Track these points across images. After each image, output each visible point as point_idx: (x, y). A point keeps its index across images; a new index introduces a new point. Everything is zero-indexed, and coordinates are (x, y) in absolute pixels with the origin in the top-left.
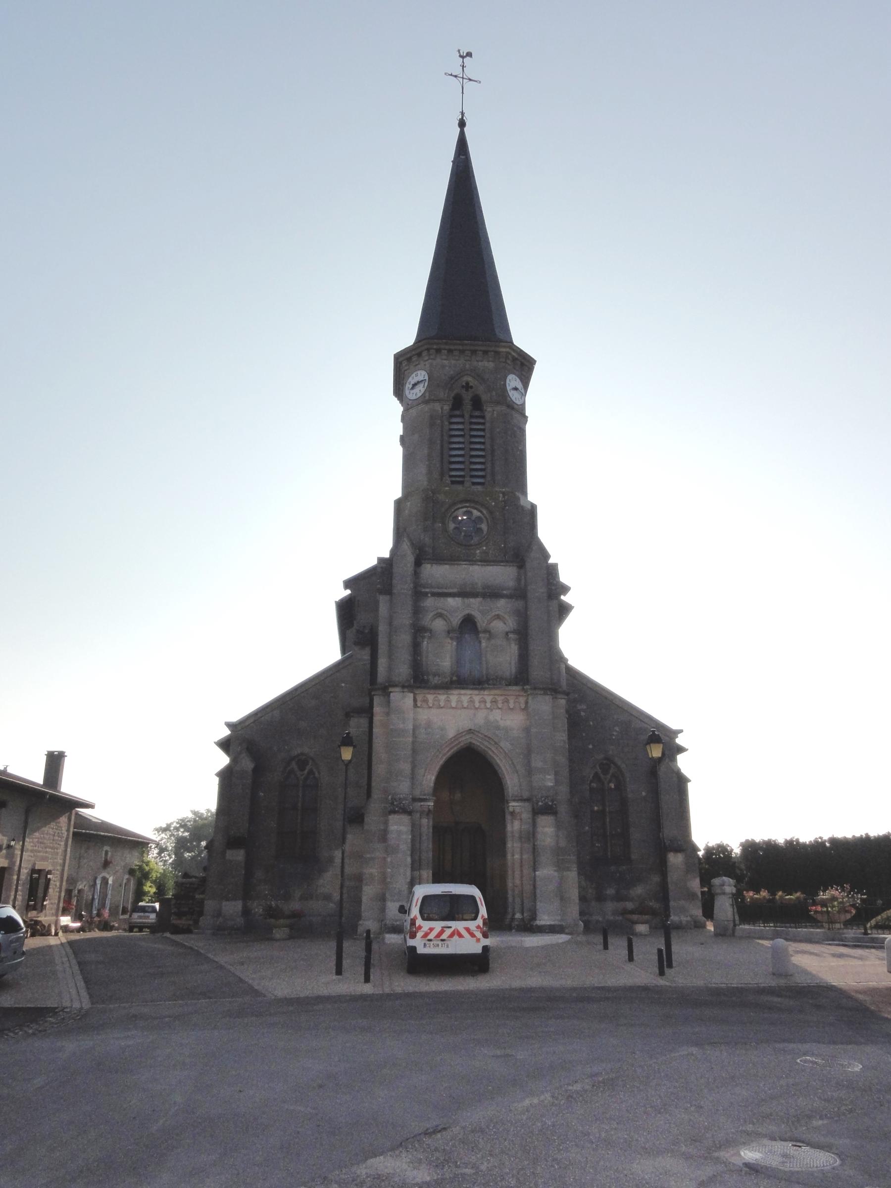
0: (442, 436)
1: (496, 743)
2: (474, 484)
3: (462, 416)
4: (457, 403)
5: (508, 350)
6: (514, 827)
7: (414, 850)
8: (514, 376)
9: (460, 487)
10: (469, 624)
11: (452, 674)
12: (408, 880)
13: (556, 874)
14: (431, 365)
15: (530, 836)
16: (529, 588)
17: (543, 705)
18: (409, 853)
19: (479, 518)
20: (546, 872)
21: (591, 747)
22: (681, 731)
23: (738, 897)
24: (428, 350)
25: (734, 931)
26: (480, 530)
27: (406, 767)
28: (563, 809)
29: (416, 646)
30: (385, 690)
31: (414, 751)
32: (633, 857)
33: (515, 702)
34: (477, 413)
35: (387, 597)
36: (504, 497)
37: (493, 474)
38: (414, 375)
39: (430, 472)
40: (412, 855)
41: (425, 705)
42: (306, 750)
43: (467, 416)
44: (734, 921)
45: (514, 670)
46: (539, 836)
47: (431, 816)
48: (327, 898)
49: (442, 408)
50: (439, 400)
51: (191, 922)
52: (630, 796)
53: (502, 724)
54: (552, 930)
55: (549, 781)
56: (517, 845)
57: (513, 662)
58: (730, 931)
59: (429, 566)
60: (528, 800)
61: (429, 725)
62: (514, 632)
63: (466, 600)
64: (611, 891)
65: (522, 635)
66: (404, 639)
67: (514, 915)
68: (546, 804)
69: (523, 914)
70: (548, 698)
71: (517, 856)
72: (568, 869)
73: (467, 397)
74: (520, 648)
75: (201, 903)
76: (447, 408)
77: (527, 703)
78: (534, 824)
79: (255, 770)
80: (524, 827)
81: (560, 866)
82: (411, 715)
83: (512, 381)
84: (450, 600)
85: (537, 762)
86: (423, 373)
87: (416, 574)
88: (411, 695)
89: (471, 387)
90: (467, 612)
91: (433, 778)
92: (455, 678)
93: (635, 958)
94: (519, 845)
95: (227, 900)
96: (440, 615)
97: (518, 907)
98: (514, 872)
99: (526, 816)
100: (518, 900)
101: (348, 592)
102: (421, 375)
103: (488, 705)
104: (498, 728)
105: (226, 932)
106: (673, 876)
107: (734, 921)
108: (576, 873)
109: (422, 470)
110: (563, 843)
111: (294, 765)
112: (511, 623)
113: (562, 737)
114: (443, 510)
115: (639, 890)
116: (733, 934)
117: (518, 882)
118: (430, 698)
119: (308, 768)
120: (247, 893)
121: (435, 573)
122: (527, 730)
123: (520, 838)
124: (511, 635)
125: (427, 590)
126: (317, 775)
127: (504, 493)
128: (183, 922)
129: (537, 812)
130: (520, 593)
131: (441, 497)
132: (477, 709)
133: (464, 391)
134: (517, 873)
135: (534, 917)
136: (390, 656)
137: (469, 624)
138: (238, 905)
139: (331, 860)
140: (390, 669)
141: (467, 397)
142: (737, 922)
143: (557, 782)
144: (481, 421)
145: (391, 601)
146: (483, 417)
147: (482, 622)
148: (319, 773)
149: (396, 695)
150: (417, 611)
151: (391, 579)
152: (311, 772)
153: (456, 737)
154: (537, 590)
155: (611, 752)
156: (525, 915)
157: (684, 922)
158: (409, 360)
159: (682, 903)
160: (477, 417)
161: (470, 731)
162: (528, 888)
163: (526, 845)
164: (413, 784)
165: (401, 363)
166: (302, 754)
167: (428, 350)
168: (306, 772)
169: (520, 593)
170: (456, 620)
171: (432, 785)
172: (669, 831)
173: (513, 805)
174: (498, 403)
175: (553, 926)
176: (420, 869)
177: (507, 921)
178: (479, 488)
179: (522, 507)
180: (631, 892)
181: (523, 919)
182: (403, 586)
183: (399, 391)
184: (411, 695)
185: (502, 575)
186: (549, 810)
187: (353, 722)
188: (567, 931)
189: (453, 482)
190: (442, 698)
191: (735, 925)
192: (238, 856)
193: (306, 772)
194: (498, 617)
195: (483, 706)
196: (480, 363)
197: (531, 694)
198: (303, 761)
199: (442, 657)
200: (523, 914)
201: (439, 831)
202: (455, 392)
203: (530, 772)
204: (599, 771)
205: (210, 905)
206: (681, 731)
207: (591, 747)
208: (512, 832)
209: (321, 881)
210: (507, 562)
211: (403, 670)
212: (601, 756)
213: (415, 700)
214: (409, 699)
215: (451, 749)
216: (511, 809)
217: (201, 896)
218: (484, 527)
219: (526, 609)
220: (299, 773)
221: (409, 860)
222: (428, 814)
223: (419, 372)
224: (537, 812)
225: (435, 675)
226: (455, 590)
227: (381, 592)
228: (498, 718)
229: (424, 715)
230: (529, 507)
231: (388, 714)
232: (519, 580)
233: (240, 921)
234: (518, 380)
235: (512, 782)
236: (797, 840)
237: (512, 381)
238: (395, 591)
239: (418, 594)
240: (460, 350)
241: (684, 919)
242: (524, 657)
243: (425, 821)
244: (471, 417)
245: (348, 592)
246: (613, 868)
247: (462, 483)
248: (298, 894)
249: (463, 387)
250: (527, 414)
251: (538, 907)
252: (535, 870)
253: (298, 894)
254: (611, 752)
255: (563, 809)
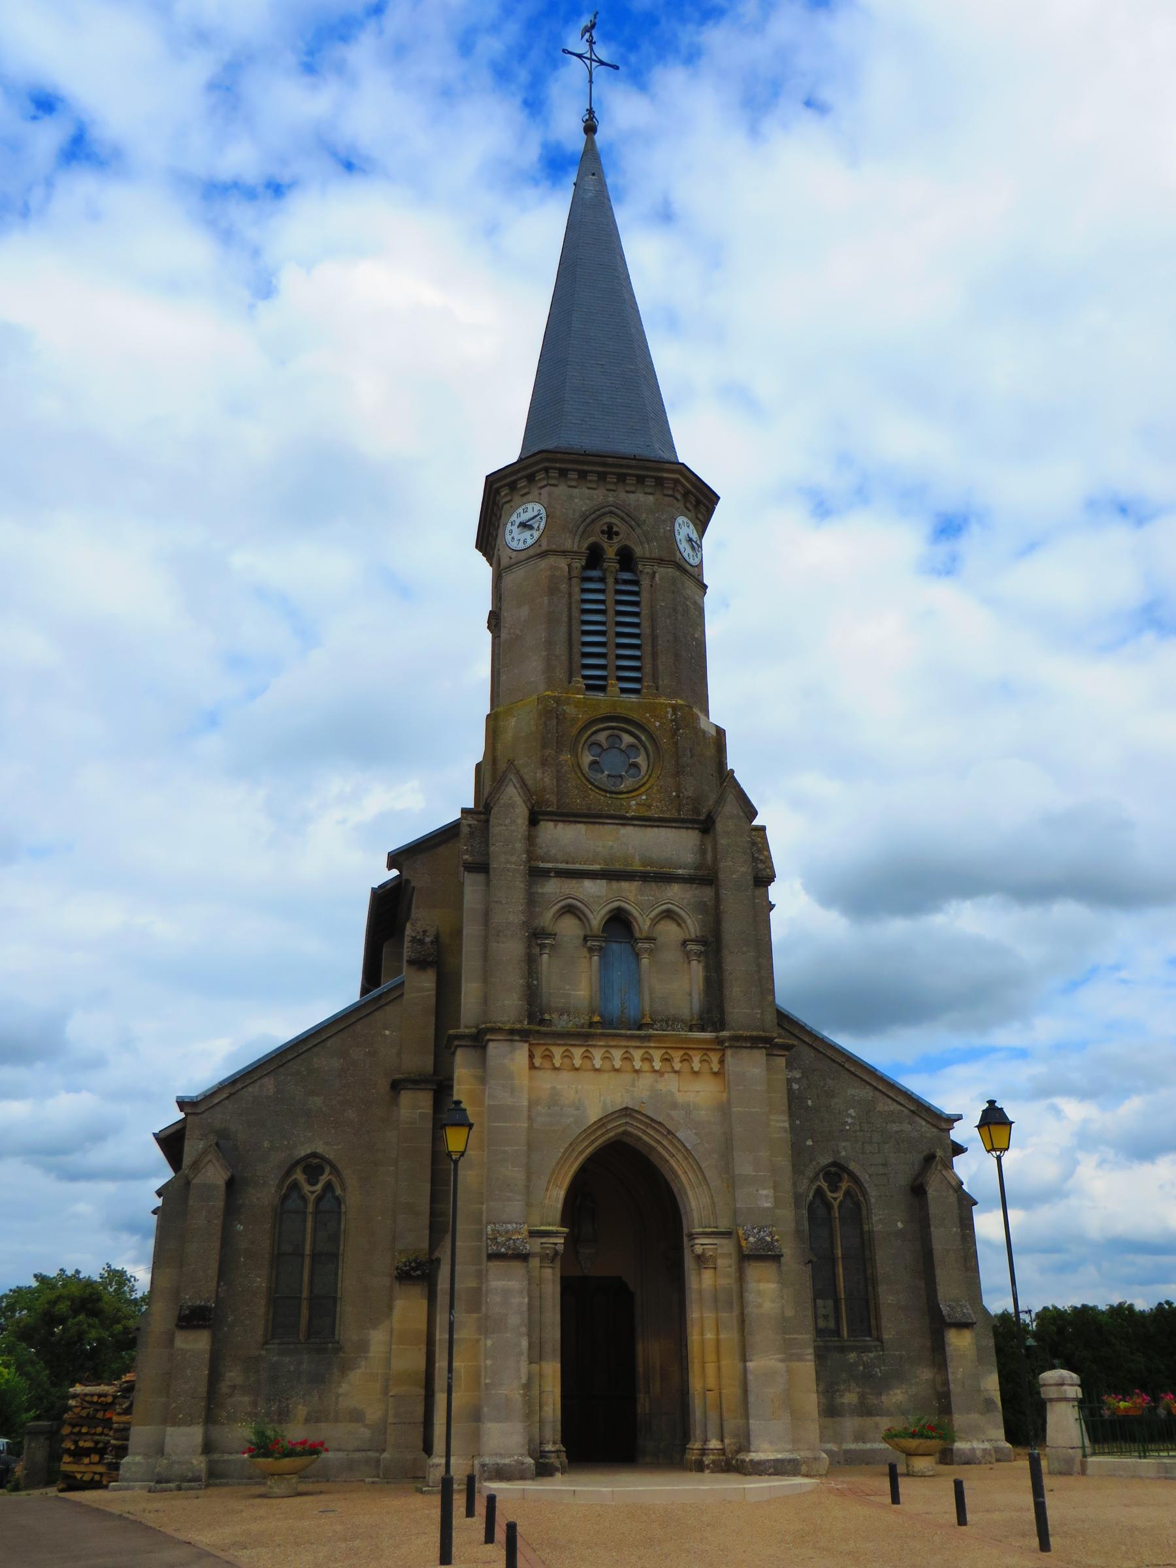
0: (570, 609)
1: (669, 1132)
2: (623, 691)
3: (602, 580)
4: (594, 557)
5: (677, 476)
6: (702, 1283)
7: (533, 1326)
8: (685, 520)
9: (600, 695)
10: (619, 922)
11: (593, 1012)
12: (524, 1381)
13: (781, 1366)
14: (550, 495)
15: (737, 1300)
16: (722, 865)
17: (751, 1067)
18: (524, 1329)
19: (632, 746)
20: (764, 1362)
21: (809, 1143)
22: (959, 1118)
23: (1088, 1406)
24: (546, 470)
25: (1083, 1465)
26: (635, 765)
27: (515, 1174)
28: (788, 1250)
29: (531, 962)
30: (478, 1040)
31: (531, 1146)
32: (886, 1337)
33: (702, 1061)
34: (626, 576)
35: (480, 877)
36: (674, 713)
37: (655, 677)
38: (520, 510)
39: (549, 668)
40: (529, 1336)
41: (547, 1064)
42: (320, 1148)
43: (610, 580)
44: (1083, 1447)
45: (696, 1005)
46: (750, 1297)
47: (558, 1264)
48: (356, 1416)
49: (569, 565)
50: (564, 553)
51: (101, 1469)
52: (878, 1228)
53: (680, 1098)
54: (779, 1468)
55: (765, 1198)
56: (710, 1316)
57: (696, 996)
58: (1077, 1467)
59: (551, 824)
60: (727, 1234)
61: (554, 1099)
62: (696, 941)
63: (615, 885)
64: (850, 1398)
65: (710, 947)
66: (511, 948)
67: (705, 1441)
68: (762, 1239)
69: (722, 1441)
70: (759, 1055)
71: (710, 1336)
72: (800, 1359)
73: (610, 552)
74: (707, 968)
75: (124, 1432)
76: (578, 564)
77: (722, 1062)
78: (741, 1278)
79: (231, 1184)
80: (724, 1282)
81: (789, 1353)
82: (526, 1082)
83: (684, 528)
84: (587, 883)
85: (744, 1167)
86: (537, 507)
87: (531, 839)
88: (526, 1046)
89: (617, 534)
90: (616, 904)
91: (562, 1194)
92: (596, 1019)
93: (969, 1517)
94: (713, 1315)
95: (174, 1424)
96: (570, 910)
97: (712, 1428)
98: (703, 1363)
99: (726, 1263)
100: (713, 1416)
101: (395, 872)
102: (531, 510)
103: (657, 1065)
104: (674, 1105)
105: (172, 1485)
106: (958, 1372)
107: (1083, 1447)
108: (812, 1364)
109: (532, 670)
110: (789, 1313)
111: (299, 1176)
112: (693, 926)
113: (780, 1122)
114: (574, 732)
115: (897, 1396)
116: (1083, 1472)
117: (711, 1382)
118: (558, 1052)
119: (324, 1179)
120: (212, 1411)
121: (562, 838)
122: (724, 1110)
123: (716, 1300)
124: (691, 947)
125: (550, 865)
126: (338, 1192)
127: (675, 708)
128: (83, 1469)
129: (745, 1258)
130: (705, 877)
131: (570, 710)
132: (637, 1071)
133: (616, 539)
134: (711, 1368)
135: (745, 1445)
136: (486, 976)
137: (619, 922)
138: (196, 1434)
139: (363, 1347)
140: (485, 1000)
141: (610, 552)
142: (1088, 1451)
143: (777, 1200)
144: (635, 589)
145: (488, 883)
146: (636, 583)
147: (643, 923)
148: (344, 1189)
149: (494, 1049)
150: (532, 901)
151: (487, 845)
152: (329, 1186)
153: (602, 1122)
154: (734, 869)
155: (843, 1153)
156: (727, 1441)
157: (979, 1453)
158: (513, 487)
159: (975, 1417)
160: (626, 582)
161: (626, 1112)
162: (731, 1391)
163: (724, 1315)
164: (529, 1205)
165: (498, 491)
166: (314, 1155)
167: (546, 470)
168: (319, 1187)
169: (705, 877)
170: (597, 920)
171: (560, 1206)
172: (948, 1292)
173: (702, 1245)
174: (661, 561)
175: (781, 1461)
176: (541, 1359)
177: (692, 1456)
178: (633, 698)
179: (704, 732)
180: (884, 1398)
181: (723, 1451)
182: (508, 854)
183: (487, 540)
184: (526, 1046)
185: (675, 846)
186: (767, 1255)
187: (406, 1097)
188: (804, 1469)
189: (589, 688)
190: (578, 1052)
191: (1085, 1456)
192: (198, 1343)
193: (319, 1187)
194: (669, 915)
195: (646, 1067)
196: (631, 496)
197: (730, 1047)
198: (313, 1166)
199: (576, 983)
200: (722, 1441)
201: (568, 1286)
202: (592, 539)
203: (732, 1181)
204: (825, 1186)
205: (140, 1435)
206: (959, 1118)
207: (809, 1143)
208: (700, 1292)
209: (344, 1388)
210: (683, 821)
211: (509, 1006)
212: (825, 1160)
213: (531, 1057)
214: (521, 1054)
215: (593, 1142)
216: (699, 1250)
217: (124, 1418)
218: (641, 760)
219: (717, 899)
220: (307, 1188)
221: (525, 1343)
222: (552, 1261)
223: (530, 506)
224: (745, 1258)
225: (562, 1012)
226: (597, 867)
227: (471, 868)
228: (674, 1089)
229: (547, 1082)
230: (713, 732)
231: (483, 1080)
232: (703, 852)
233: (199, 1463)
234: (692, 526)
235: (697, 1205)
236: (1055, 1308)
237: (684, 528)
238: (494, 865)
239: (536, 874)
240: (598, 473)
241: (978, 1446)
242: (715, 985)
243: (548, 1272)
244: (617, 582)
245: (395, 872)
246: (852, 1356)
247: (602, 689)
248: (302, 1411)
249: (603, 532)
250: (705, 582)
251: (752, 1427)
252: (744, 1359)
253: (302, 1411)
254: (843, 1153)
255: (788, 1250)
